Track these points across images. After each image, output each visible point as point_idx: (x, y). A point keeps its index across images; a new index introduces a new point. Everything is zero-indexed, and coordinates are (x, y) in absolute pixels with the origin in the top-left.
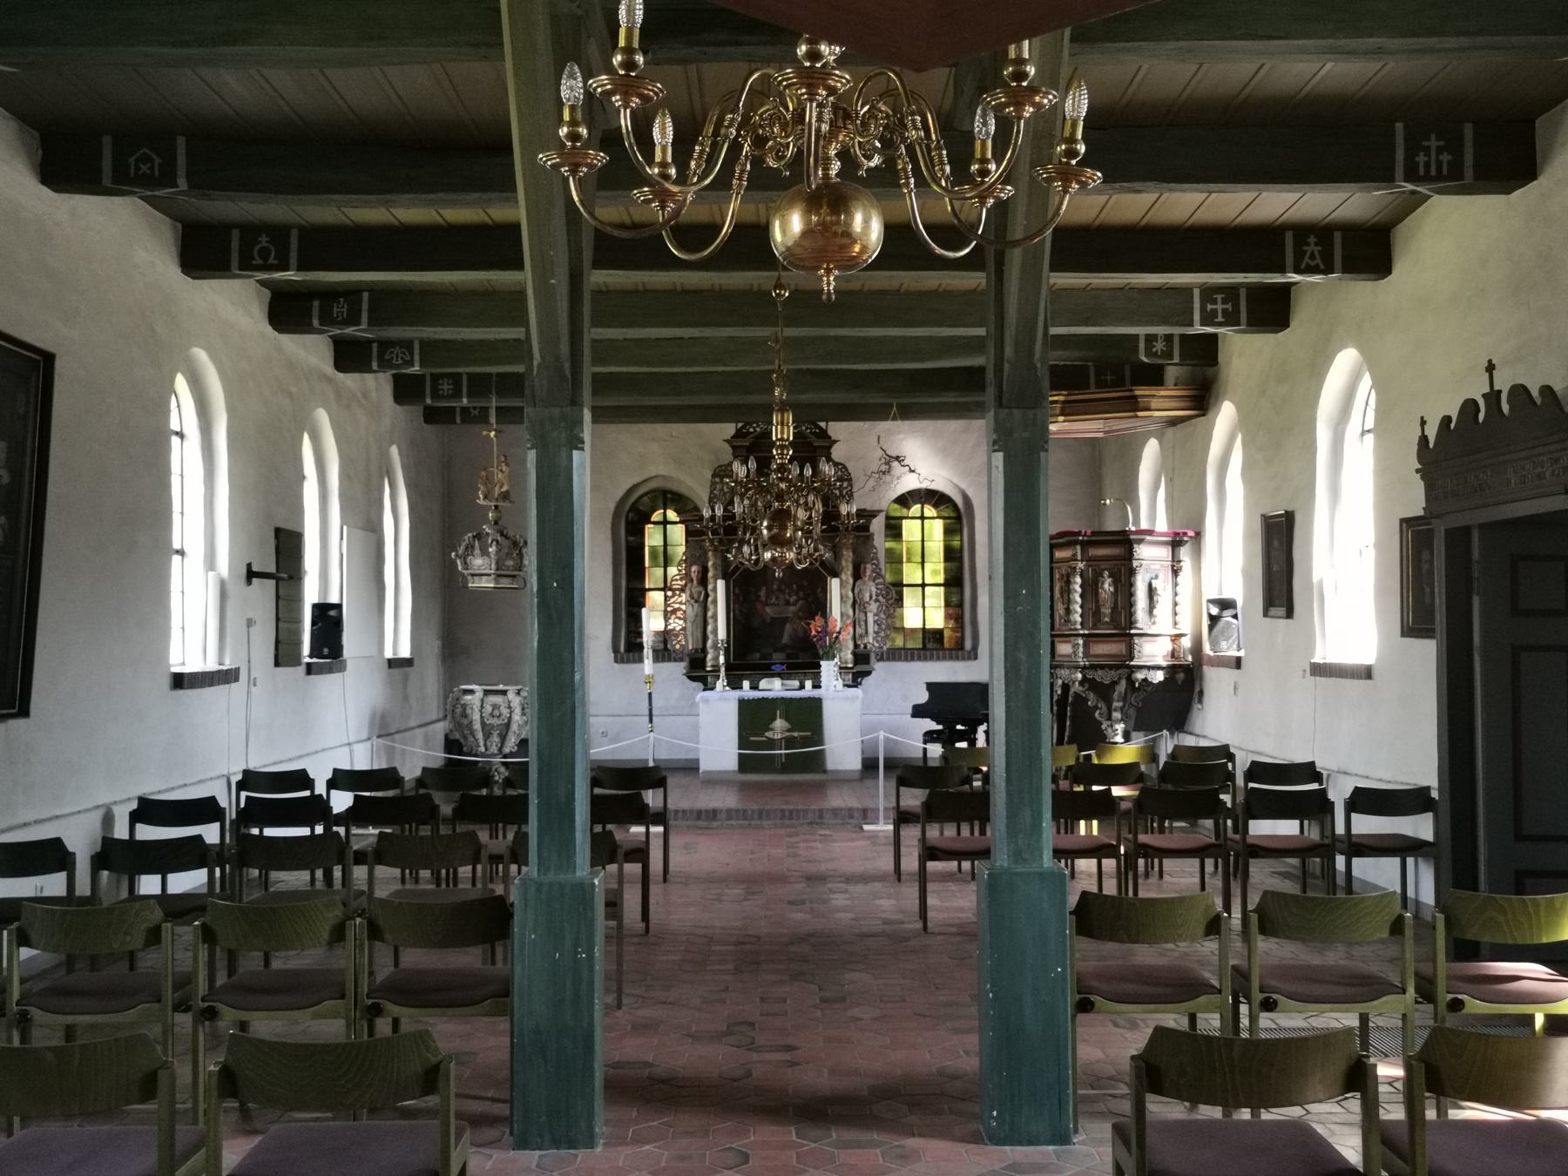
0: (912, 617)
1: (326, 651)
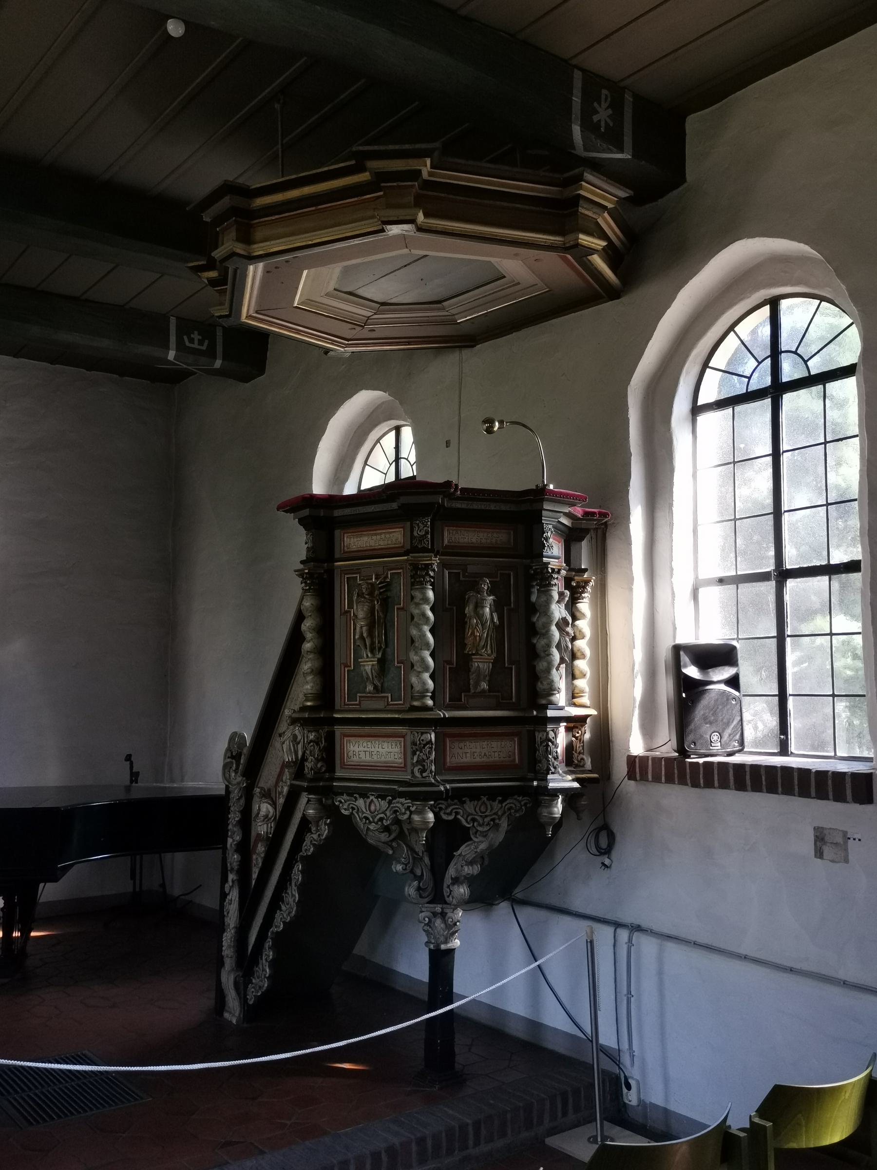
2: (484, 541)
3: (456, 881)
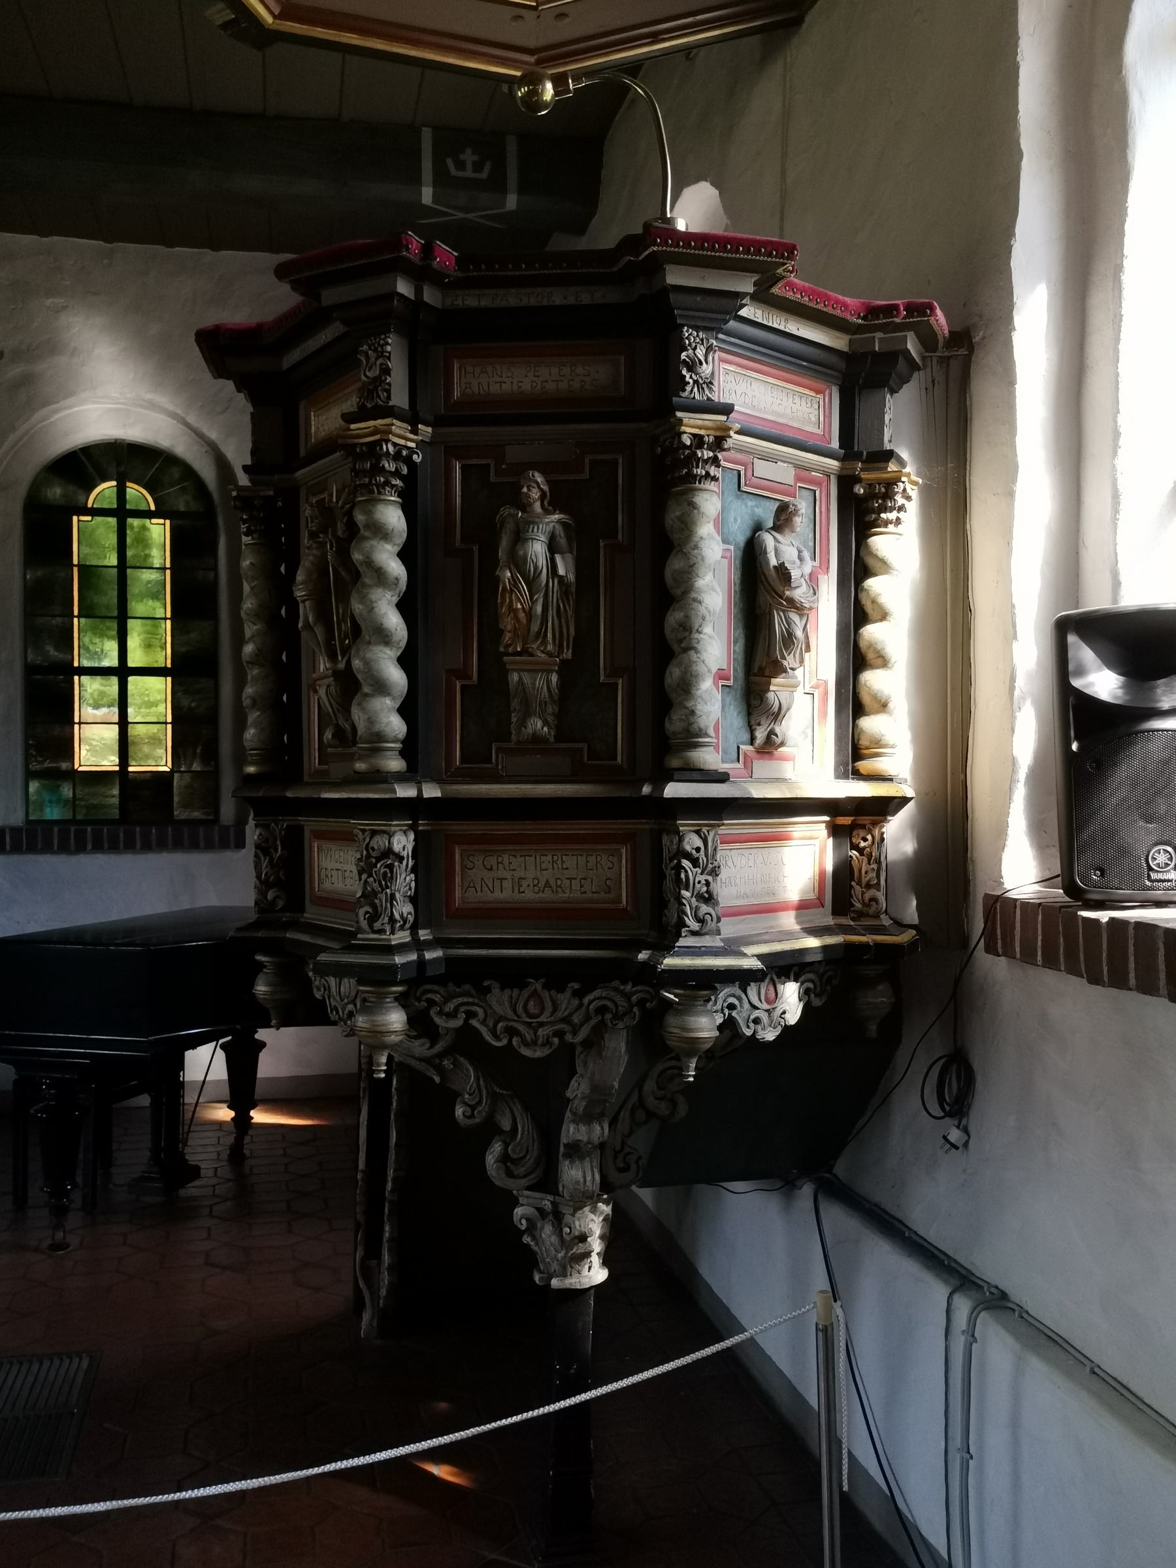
2: (551, 386)
3: (575, 1151)
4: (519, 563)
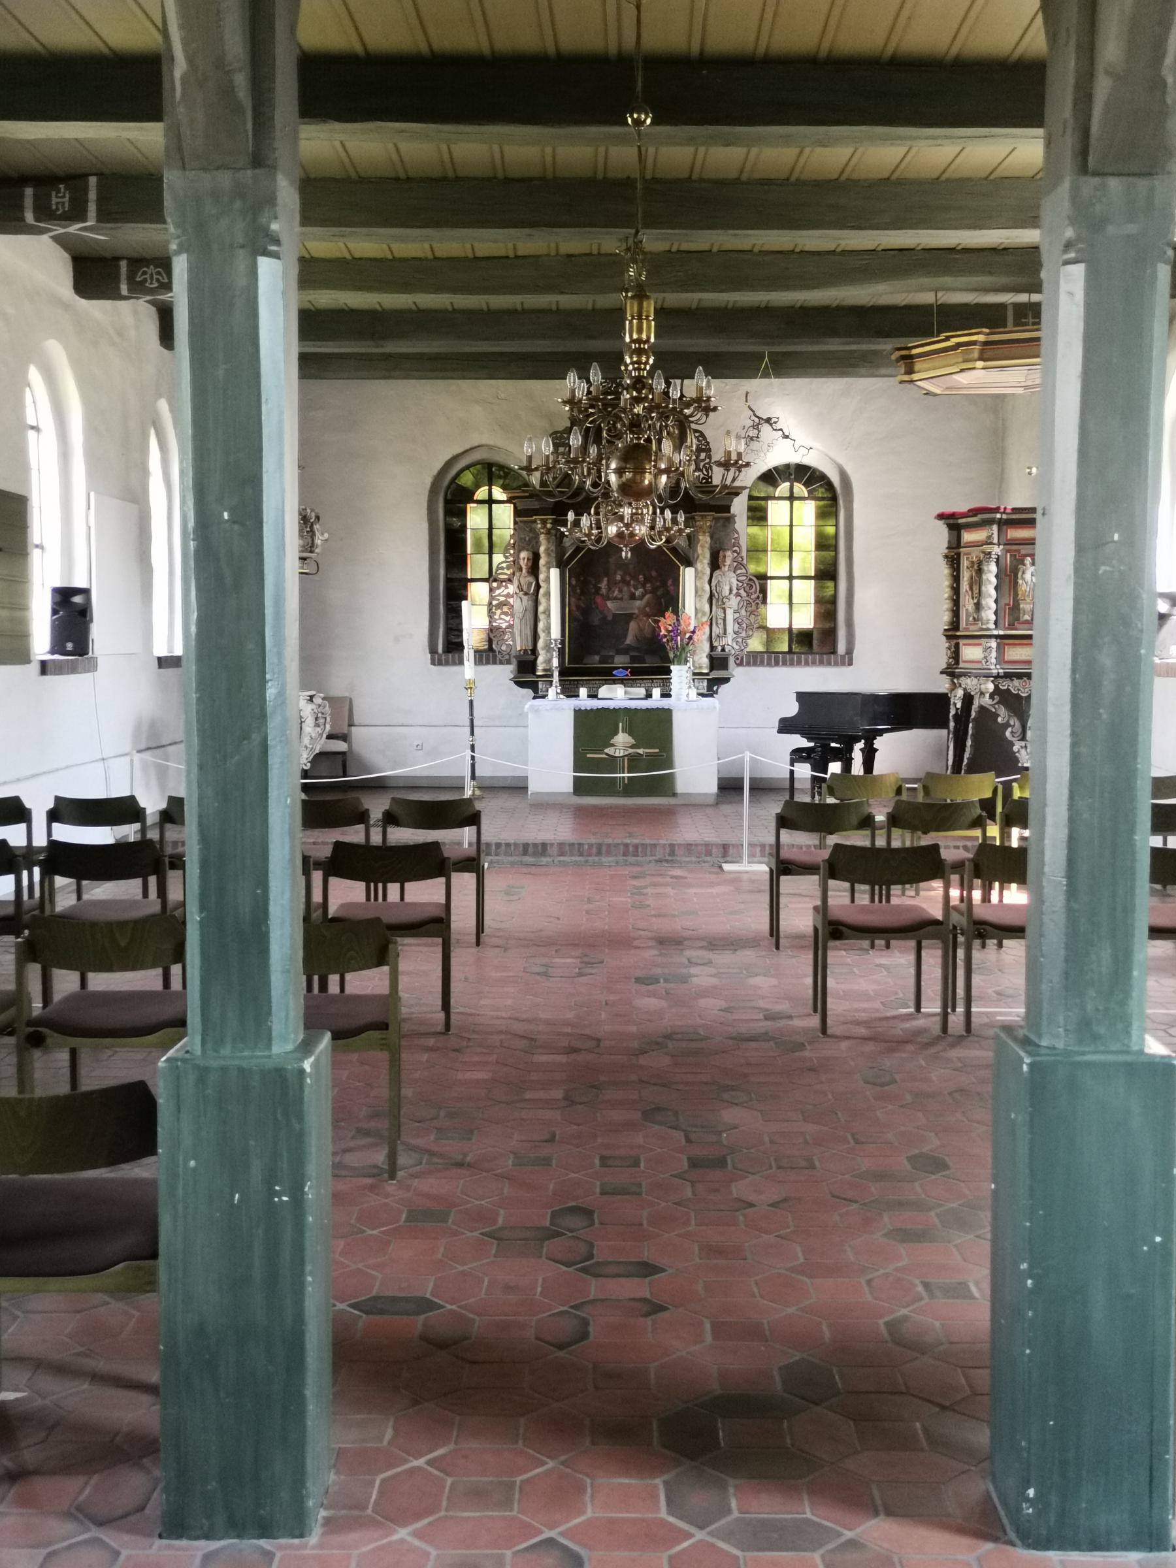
0: (776, 615)
1: (69, 646)
4: (1023, 579)
